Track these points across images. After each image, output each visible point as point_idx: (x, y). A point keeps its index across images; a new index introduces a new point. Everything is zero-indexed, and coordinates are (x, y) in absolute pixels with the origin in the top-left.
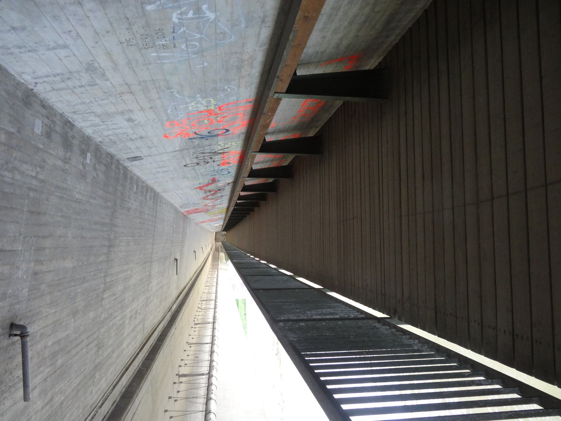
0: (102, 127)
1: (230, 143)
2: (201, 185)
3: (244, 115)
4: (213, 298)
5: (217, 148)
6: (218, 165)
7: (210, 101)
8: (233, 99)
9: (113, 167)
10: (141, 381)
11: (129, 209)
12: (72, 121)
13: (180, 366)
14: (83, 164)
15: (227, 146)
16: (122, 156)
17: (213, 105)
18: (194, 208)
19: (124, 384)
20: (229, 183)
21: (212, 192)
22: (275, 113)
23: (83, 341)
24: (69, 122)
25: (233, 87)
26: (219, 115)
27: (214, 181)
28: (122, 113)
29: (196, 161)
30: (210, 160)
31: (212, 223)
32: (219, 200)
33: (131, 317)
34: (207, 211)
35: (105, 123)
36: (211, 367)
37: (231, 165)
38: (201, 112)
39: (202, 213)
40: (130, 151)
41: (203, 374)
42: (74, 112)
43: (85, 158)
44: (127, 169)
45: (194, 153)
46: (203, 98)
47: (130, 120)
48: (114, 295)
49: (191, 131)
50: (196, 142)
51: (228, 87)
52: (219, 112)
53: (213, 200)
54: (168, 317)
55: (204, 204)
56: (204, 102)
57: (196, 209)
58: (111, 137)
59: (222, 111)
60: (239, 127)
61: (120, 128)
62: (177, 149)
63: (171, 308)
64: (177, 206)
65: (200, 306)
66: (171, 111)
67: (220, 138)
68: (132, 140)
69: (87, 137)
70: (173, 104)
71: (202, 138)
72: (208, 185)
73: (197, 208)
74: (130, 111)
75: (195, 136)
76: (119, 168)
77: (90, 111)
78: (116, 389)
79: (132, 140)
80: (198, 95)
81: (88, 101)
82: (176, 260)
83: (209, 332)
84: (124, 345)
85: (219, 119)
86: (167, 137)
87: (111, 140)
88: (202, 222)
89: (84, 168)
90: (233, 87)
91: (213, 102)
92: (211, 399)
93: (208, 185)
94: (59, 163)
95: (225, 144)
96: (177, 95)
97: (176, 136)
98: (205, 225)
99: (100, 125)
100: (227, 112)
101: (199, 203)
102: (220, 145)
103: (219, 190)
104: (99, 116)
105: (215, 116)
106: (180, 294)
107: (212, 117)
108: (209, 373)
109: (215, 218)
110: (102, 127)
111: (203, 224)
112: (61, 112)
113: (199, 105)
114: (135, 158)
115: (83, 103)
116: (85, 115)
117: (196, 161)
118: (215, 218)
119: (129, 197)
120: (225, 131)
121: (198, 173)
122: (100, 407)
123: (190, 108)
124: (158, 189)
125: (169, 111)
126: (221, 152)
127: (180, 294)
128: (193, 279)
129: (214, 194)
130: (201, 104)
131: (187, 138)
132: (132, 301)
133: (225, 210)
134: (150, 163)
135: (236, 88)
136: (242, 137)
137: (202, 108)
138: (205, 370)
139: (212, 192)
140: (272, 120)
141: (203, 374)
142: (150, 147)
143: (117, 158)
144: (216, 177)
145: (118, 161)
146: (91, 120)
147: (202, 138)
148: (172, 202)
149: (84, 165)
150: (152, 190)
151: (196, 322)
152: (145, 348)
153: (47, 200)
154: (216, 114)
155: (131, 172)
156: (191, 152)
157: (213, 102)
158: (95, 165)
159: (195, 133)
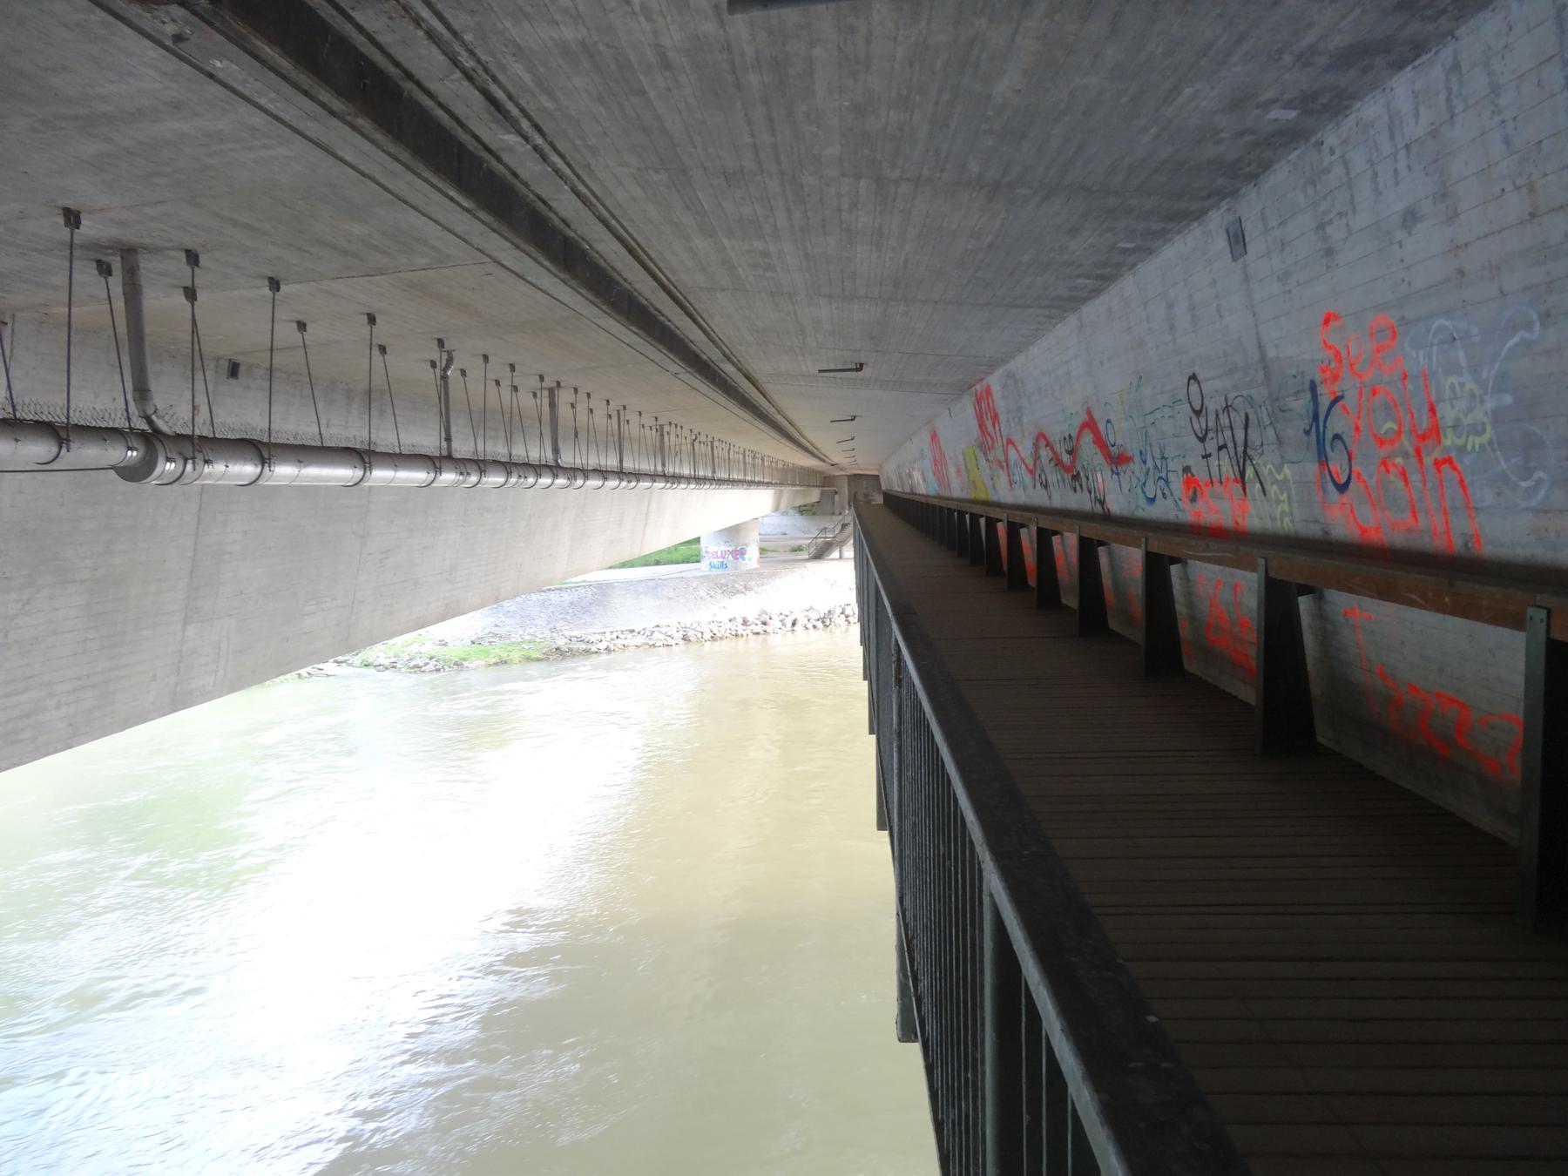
0: (1387, 148)
1: (1284, 497)
2: (1102, 427)
3: (1409, 531)
4: (719, 475)
5: (1266, 464)
6: (1187, 469)
7: (1480, 433)
8: (1485, 496)
9: (1221, 182)
10: (590, 289)
11: (1074, 231)
12: (1417, 63)
13: (576, 390)
14: (1273, 101)
15: (1273, 490)
16: (1252, 205)
17: (1460, 442)
18: (1001, 411)
19: (600, 247)
20: (1102, 503)
21: (1066, 459)
22: (1453, 613)
23: (773, 133)
24: (1418, 56)
25: (1542, 494)
26: (1414, 460)
27: (1118, 460)
28: (1443, 195)
29: (1213, 405)
30: (1211, 446)
31: (928, 463)
32: (1027, 478)
33: (765, 254)
34: (985, 448)
35: (1403, 153)
36: (574, 472)
37: (1187, 506)
38: (1432, 410)
39: (976, 432)
40: (1273, 223)
41: (556, 451)
42: (1456, 66)
43: (1288, 106)
44: (1197, 219)
45: (1249, 400)
46: (1497, 416)
47: (1411, 217)
48: (854, 205)
49: (1348, 385)
50: (1301, 404)
51: (1540, 481)
52: (1428, 461)
53: (1030, 462)
54: (710, 353)
55: (1015, 438)
56: (1478, 415)
57: (995, 418)
58: (1338, 171)
59: (1433, 470)
60: (1345, 519)
61: (1377, 192)
62: (1271, 353)
63: (728, 359)
64: (1018, 364)
65: (702, 438)
66: (1441, 329)
67: (1312, 468)
68: (1321, 227)
69: (1349, 107)
70: (1475, 330)
71: (1316, 417)
72: (1100, 442)
73: (1002, 418)
74: (1453, 217)
75: (1325, 401)
76: (1209, 196)
77: (1459, 108)
78: (600, 227)
79: (1321, 227)
80: (1508, 399)
81: (1502, 101)
82: (860, 367)
83: (646, 466)
84: (699, 242)
85: (1399, 460)
86: (1327, 321)
87: (1327, 171)
88: (934, 437)
89: (1258, 106)
90: (1542, 494)
91: (1475, 442)
92: (509, 474)
93: (1100, 442)
94: (1309, 39)
95: (1283, 485)
96: (1516, 339)
97: (1330, 347)
98: (922, 441)
99: (1392, 137)
100: (1424, 482)
101: (1020, 423)
102: (1279, 469)
103: (1076, 477)
104: (1434, 133)
105: (1411, 451)
106: (754, 383)
107: (1407, 443)
108: (558, 466)
109: (952, 470)
110: (1387, 148)
111: (927, 439)
112: (1458, 33)
113: (1462, 404)
114: (1238, 241)
115: (1495, 89)
116: (1443, 96)
117: (1213, 405)
118: (952, 470)
119: (1109, 230)
120: (1343, 479)
121: (1158, 414)
122: (575, 191)
123: (1453, 379)
124: (1091, 310)
125: (1442, 321)
126: (1250, 472)
127: (754, 383)
128: (779, 418)
129: (1059, 463)
130: (1470, 410)
131: (1318, 377)
132: (806, 256)
133: (982, 496)
134: (1214, 282)
135: (1533, 503)
136: (1314, 531)
137: (1447, 413)
138: (567, 459)
139: (1066, 459)
140: (1420, 606)
141: (556, 451)
142: (1284, 277)
143: (1243, 191)
144: (1136, 466)
145: (1234, 193)
146: (1417, 114)
147: (1316, 417)
148: (1034, 350)
149: (1266, 106)
150: (1096, 292)
151: (666, 429)
152: (664, 295)
153: (1220, 16)
154: (1418, 451)
155: (1179, 232)
156: (1253, 392)
157: (1475, 442)
158: (1253, 133)
159: (1337, 399)
